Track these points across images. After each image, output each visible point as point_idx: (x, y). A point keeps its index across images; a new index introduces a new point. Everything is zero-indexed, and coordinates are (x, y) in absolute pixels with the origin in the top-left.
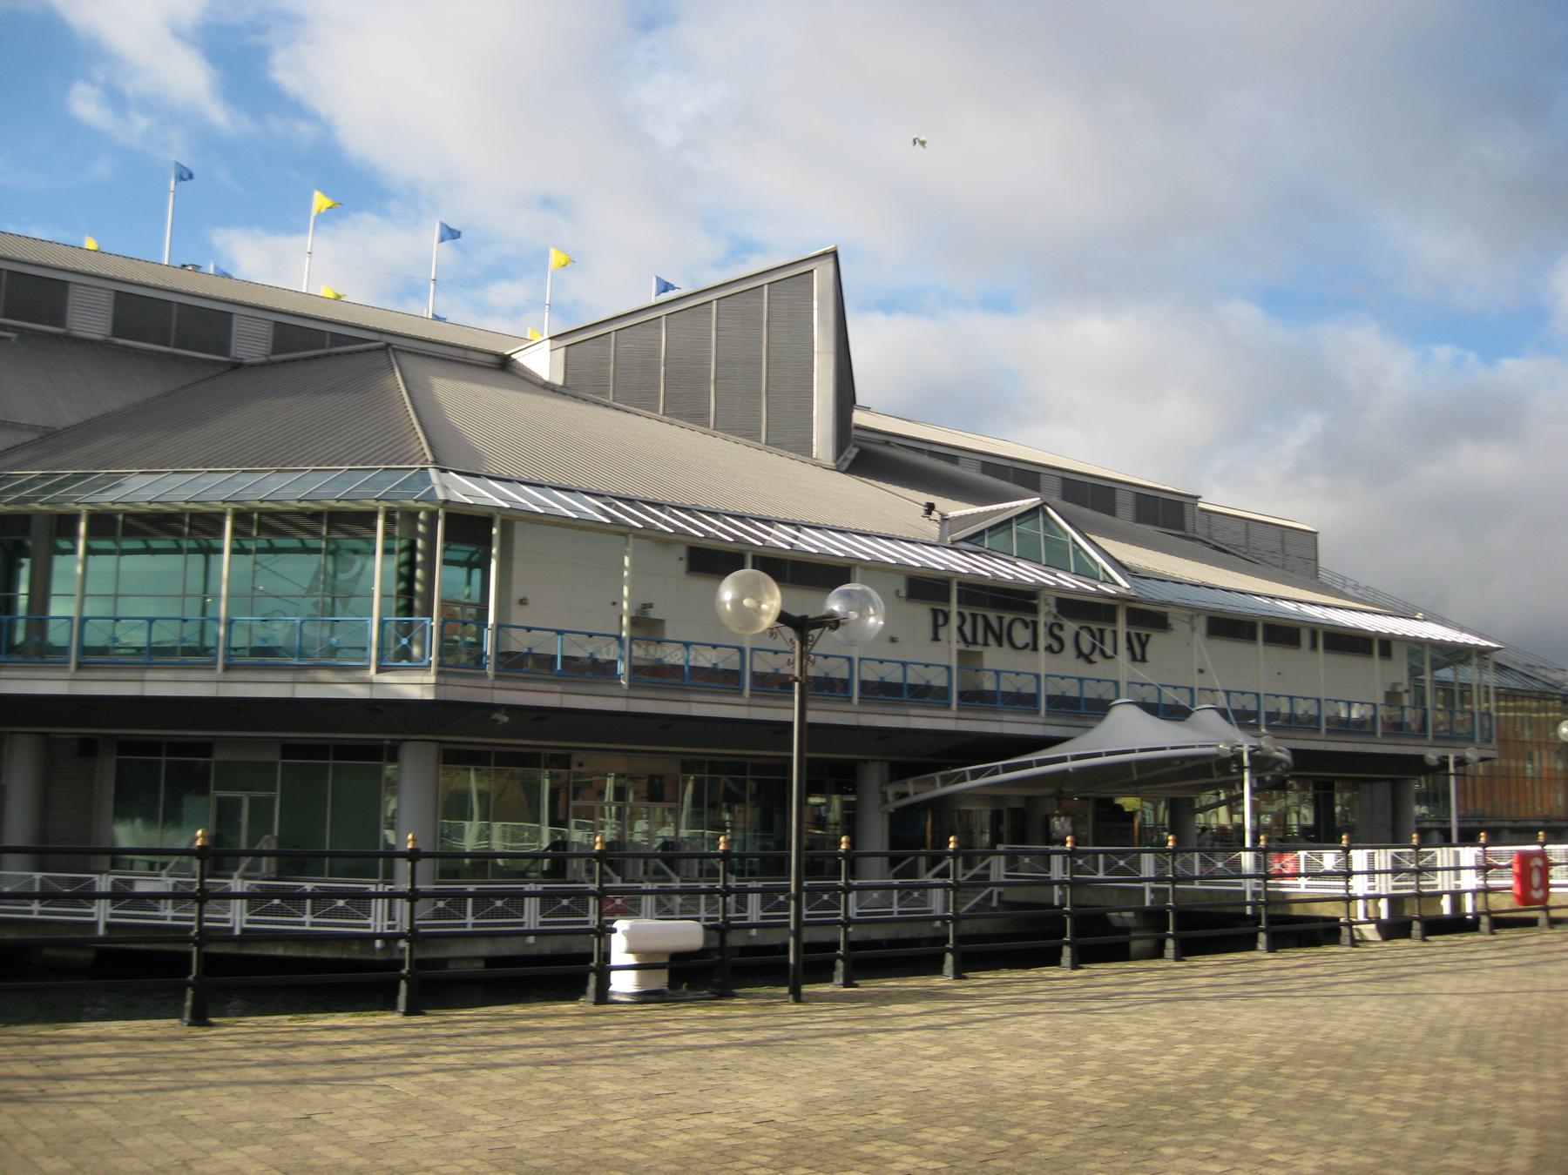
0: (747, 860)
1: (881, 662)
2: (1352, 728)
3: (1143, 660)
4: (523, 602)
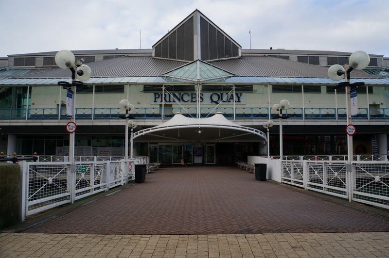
0: (215, 163)
1: (312, 109)
2: (320, 117)
3: (239, 101)
4: (33, 104)
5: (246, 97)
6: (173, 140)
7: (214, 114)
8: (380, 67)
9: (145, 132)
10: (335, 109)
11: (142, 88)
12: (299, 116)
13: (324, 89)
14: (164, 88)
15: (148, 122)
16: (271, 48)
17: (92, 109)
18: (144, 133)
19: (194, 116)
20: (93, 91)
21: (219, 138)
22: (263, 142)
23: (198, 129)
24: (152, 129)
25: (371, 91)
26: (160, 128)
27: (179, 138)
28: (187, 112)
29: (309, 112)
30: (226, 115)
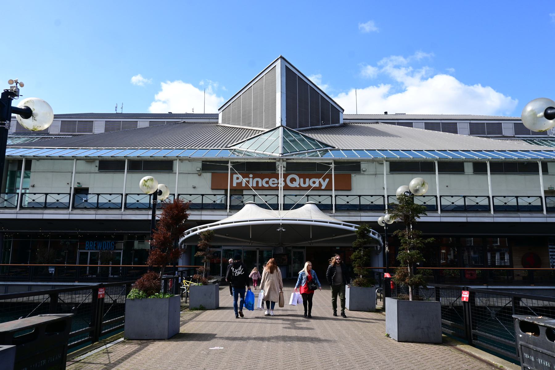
4: (33, 186)
6: (245, 242)
7: (303, 205)
8: (551, 136)
9: (210, 228)
11: (200, 165)
13: (99, 128)
14: (230, 166)
15: (206, 215)
16: (386, 113)
17: (122, 194)
18: (199, 231)
19: (275, 207)
20: (124, 169)
21: (311, 240)
22: (377, 247)
23: (278, 225)
24: (211, 226)
25: (545, 171)
26: (222, 224)
27: (251, 239)
28: (263, 200)
29: (446, 202)
30: (324, 208)
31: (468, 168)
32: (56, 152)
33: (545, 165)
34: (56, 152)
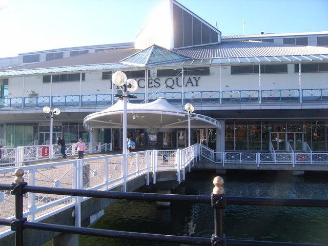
5: (203, 80)
10: (298, 90)
12: (215, 100)
13: (43, 59)
31: (291, 68)
32: (19, 72)
33: (84, 75)
34: (19, 72)
